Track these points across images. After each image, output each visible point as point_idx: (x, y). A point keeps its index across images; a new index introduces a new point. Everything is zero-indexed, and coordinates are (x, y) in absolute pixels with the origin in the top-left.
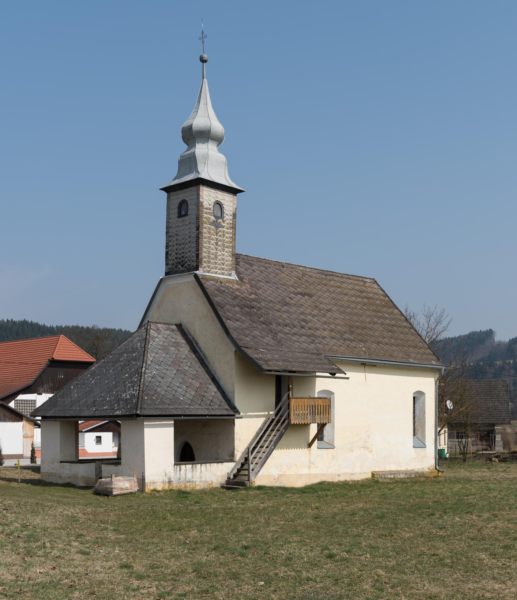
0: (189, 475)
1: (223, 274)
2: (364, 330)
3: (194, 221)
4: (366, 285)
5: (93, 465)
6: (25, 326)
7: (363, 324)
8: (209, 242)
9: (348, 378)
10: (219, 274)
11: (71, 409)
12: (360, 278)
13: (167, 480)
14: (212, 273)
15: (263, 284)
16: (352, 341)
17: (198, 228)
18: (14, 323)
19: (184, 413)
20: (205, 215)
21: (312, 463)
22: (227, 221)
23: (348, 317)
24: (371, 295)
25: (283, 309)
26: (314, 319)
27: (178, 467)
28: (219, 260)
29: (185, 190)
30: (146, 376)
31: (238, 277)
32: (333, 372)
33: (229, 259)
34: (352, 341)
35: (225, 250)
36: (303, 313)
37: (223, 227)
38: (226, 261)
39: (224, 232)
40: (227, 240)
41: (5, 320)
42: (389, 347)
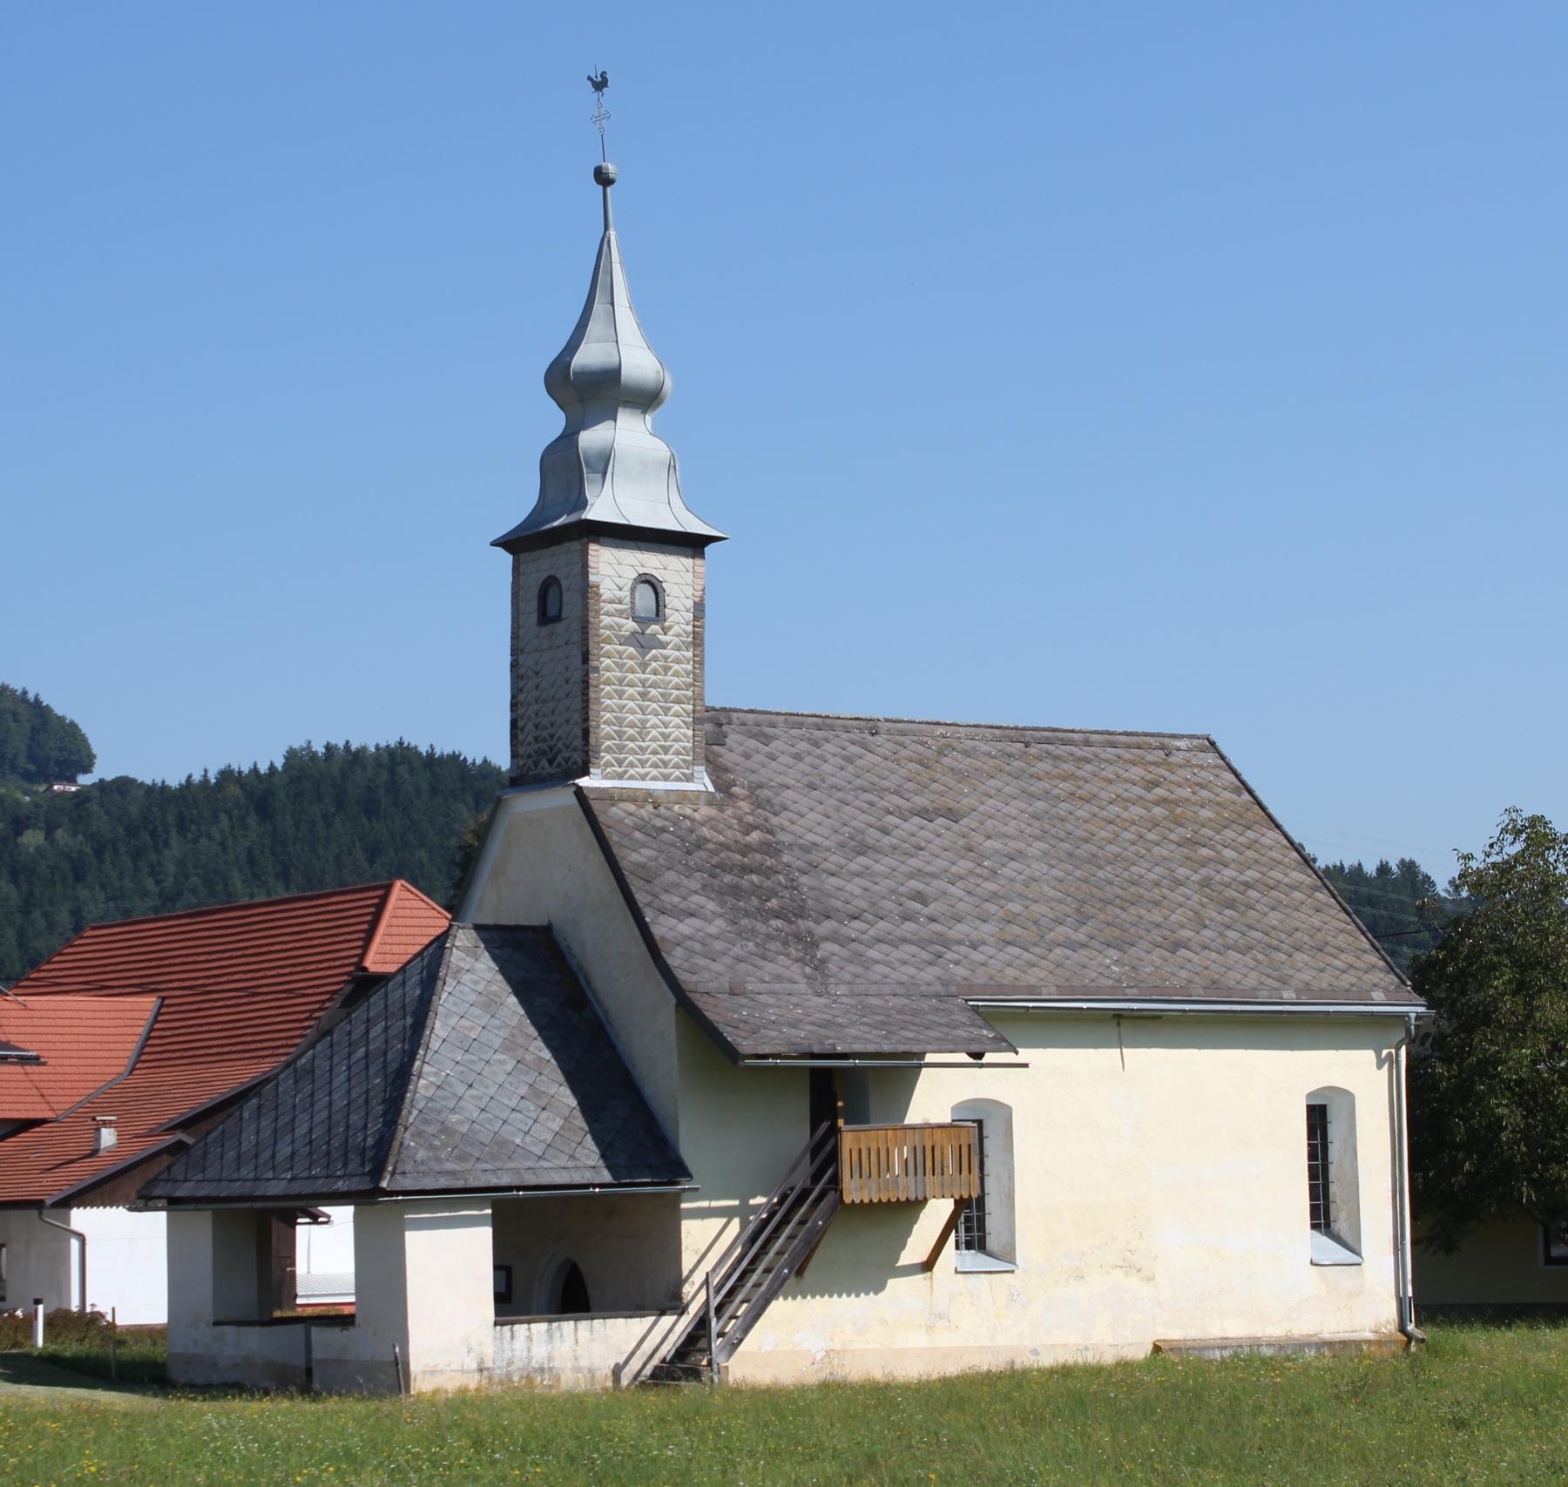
0: (540, 1352)
1: (666, 778)
2: (1132, 910)
3: (577, 637)
4: (1171, 759)
5: (300, 1327)
6: (402, 770)
7: (1133, 889)
8: (620, 695)
9: (1026, 1065)
10: (654, 779)
11: (235, 1176)
12: (1152, 740)
13: (475, 1366)
14: (632, 778)
15: (797, 797)
16: (1073, 946)
17: (586, 658)
18: (355, 758)
19: (517, 1182)
20: (606, 620)
21: (940, 1316)
22: (676, 629)
23: (1078, 873)
24: (1185, 793)
25: (853, 866)
26: (952, 889)
27: (507, 1328)
28: (654, 740)
29: (554, 548)
30: (422, 1082)
31: (713, 782)
32: (975, 1048)
33: (680, 732)
34: (1073, 946)
35: (669, 709)
36: (918, 874)
37: (663, 646)
38: (676, 740)
39: (666, 658)
40: (676, 680)
41: (319, 748)
42: (1214, 955)
